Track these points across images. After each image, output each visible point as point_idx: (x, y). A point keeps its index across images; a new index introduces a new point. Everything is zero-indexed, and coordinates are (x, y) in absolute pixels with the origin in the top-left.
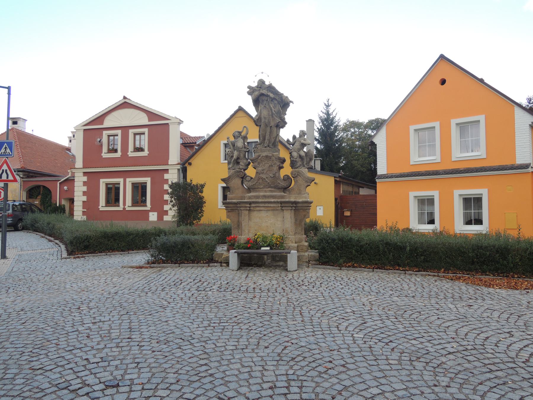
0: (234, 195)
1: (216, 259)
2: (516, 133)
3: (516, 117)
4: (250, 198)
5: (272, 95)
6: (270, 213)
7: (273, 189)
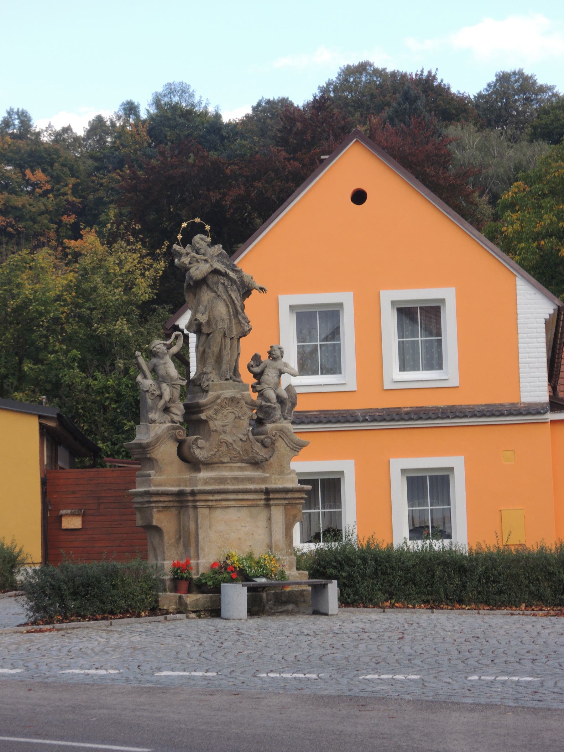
0: (163, 477)
1: (165, 608)
2: (520, 335)
3: (520, 299)
4: (206, 482)
5: (232, 274)
6: (244, 513)
7: (244, 465)
